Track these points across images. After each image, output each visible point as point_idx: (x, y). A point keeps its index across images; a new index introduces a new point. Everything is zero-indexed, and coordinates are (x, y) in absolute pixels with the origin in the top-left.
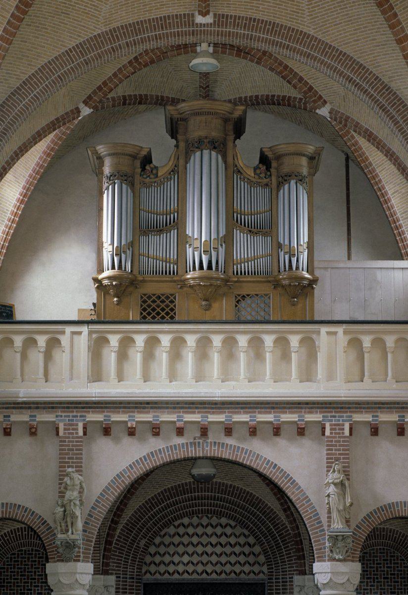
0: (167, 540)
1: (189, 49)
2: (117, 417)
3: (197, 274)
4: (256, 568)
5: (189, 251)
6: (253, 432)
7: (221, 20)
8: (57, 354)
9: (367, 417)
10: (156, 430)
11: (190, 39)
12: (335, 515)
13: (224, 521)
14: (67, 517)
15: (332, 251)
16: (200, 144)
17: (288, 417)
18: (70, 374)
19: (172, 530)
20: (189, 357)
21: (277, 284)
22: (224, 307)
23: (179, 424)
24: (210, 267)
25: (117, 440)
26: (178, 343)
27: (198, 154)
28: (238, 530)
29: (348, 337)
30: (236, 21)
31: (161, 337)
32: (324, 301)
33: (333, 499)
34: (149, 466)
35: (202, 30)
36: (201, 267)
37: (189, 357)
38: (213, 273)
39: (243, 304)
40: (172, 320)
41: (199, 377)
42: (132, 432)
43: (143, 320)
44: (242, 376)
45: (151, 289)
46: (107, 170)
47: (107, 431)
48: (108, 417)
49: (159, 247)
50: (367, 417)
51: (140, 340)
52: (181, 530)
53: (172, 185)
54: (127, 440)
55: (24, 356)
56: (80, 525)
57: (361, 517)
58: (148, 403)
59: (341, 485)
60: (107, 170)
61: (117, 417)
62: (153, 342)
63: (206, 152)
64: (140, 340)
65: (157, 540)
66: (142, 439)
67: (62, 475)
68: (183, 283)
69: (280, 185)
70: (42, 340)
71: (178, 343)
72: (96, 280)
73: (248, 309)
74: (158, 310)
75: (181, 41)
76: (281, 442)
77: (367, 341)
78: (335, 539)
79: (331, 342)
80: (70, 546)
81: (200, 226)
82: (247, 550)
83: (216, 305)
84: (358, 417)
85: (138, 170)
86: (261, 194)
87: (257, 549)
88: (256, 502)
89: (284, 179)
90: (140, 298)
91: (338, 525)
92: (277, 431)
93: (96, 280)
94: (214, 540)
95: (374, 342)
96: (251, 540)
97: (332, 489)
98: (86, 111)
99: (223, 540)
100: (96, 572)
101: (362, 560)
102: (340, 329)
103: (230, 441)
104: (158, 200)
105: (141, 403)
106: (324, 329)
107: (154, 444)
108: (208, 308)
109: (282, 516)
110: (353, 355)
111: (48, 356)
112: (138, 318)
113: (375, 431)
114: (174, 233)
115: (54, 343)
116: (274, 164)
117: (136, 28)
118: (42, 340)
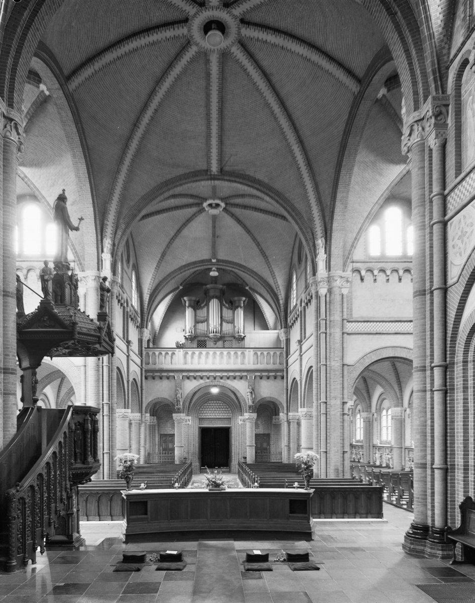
0: (205, 407)
1: (210, 270)
2: (163, 374)
3: (212, 334)
4: (229, 414)
5: (210, 328)
6: (228, 378)
7: (218, 261)
8: (174, 356)
9: (259, 374)
10: (202, 378)
11: (210, 267)
12: (250, 400)
13: (220, 402)
14: (178, 401)
15: (250, 327)
16: (213, 297)
17: (237, 374)
18: (179, 361)
19: (206, 404)
20: (218, 357)
21: (234, 337)
22: (220, 343)
23: (221, 376)
24: (216, 332)
25: (191, 380)
26: (208, 353)
27: (212, 300)
28: (224, 404)
29: (254, 352)
30: (223, 261)
31: (210, 352)
32: (247, 342)
33: (249, 397)
34: (200, 387)
35: (214, 264)
36: (214, 332)
37: (218, 357)
38: (217, 334)
39: (225, 343)
40: (206, 348)
41: (206, 363)
42: (195, 378)
43: (198, 348)
44: (225, 362)
45: (200, 339)
46: (187, 305)
47: (188, 378)
48: (189, 374)
49: (202, 327)
50: (259, 374)
51: (197, 353)
52: (209, 404)
53: (205, 309)
54: (194, 381)
55: (165, 357)
56: (181, 404)
57: (257, 401)
58: (200, 370)
59: (251, 393)
60: (187, 305)
61: (163, 374)
62: (201, 353)
63: (215, 300)
64: (197, 353)
65: (202, 407)
66: (198, 380)
67: (176, 390)
68: (209, 337)
69: (235, 309)
70: (170, 353)
71: (208, 353)
72: (184, 336)
73: (227, 344)
74: (202, 344)
75: (207, 267)
76: (235, 381)
77: (259, 353)
78: (250, 407)
79: (249, 354)
80: (179, 409)
81: (214, 322)
82: (226, 409)
83: (218, 343)
84: (257, 374)
85: (196, 306)
86: (230, 312)
87: (229, 409)
88: (229, 397)
89: (237, 307)
90: (198, 341)
91: (251, 403)
92: (235, 378)
93: (184, 336)
94: (217, 407)
95: (242, 353)
96: (228, 407)
97: (249, 394)
98: (181, 288)
99: (220, 407)
100: (150, 416)
101: (257, 412)
102: (252, 350)
103: (222, 381)
104: (202, 313)
105: (183, 370)
106: (247, 350)
107: (202, 381)
108: (216, 344)
109: (236, 400)
110: (255, 356)
111: (172, 358)
112: (196, 347)
113: (261, 378)
114: (206, 323)
115: (173, 354)
116: (234, 303)
117: (194, 263)
118: (170, 353)
